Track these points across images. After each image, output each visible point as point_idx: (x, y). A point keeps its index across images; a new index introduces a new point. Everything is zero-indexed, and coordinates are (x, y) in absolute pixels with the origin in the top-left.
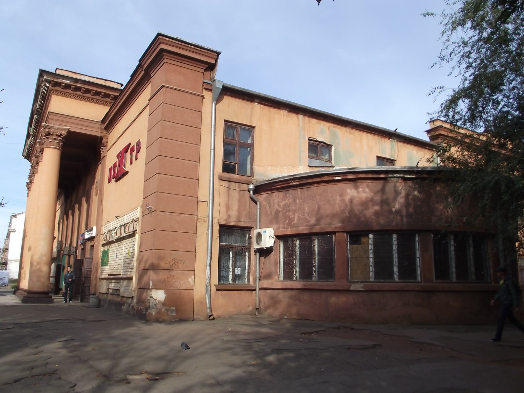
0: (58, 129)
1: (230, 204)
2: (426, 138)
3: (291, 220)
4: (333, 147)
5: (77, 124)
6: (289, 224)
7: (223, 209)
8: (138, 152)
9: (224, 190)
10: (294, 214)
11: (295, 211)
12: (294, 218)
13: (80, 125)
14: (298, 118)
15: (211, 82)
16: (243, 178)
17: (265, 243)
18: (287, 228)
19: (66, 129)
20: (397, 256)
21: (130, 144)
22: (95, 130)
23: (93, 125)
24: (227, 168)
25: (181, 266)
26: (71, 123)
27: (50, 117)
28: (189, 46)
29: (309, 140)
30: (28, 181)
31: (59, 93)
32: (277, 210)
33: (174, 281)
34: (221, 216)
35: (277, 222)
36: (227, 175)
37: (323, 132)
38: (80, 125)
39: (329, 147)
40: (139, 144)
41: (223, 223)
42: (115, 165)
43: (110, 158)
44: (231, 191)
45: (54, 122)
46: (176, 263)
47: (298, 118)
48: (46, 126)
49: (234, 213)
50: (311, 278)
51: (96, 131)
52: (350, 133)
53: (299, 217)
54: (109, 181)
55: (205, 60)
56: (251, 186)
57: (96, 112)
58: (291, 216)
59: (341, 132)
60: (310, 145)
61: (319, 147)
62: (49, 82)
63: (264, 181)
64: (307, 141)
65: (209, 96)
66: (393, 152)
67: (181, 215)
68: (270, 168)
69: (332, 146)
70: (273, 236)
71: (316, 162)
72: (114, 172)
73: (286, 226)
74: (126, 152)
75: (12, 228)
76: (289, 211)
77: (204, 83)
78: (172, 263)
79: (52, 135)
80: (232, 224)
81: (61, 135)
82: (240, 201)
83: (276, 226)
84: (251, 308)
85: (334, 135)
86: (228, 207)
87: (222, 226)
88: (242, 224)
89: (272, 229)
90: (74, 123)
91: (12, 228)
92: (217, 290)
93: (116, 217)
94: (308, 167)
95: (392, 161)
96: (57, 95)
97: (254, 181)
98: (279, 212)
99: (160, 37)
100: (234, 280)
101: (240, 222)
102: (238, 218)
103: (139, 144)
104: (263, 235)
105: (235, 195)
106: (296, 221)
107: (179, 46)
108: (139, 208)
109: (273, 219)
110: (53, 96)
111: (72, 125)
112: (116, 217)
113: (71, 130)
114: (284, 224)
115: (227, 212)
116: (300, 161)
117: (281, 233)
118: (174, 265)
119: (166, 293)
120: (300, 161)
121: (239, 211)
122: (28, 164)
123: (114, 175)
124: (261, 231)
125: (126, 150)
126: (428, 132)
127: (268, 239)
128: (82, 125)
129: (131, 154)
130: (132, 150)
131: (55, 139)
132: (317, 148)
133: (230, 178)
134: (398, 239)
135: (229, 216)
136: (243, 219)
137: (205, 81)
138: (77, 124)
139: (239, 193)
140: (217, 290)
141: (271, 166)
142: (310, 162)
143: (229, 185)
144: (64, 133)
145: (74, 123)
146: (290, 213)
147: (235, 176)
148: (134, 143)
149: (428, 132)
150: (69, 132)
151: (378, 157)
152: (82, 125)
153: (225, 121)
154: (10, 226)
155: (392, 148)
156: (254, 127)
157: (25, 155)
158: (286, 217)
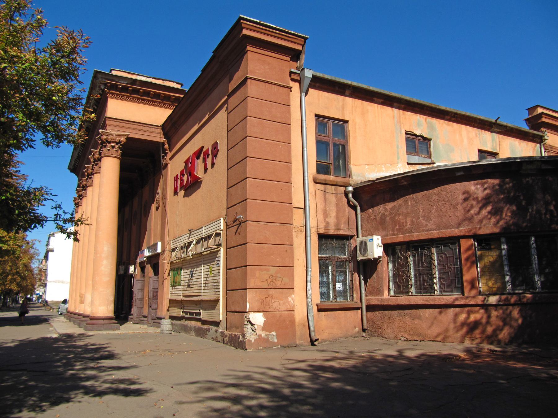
0: (116, 135)
1: (327, 209)
2: (525, 128)
3: (402, 225)
4: (432, 142)
5: (137, 129)
6: (400, 231)
7: (321, 216)
8: (215, 155)
9: (319, 194)
10: (406, 218)
11: (406, 215)
12: (406, 222)
13: (139, 130)
14: (393, 111)
15: (299, 72)
16: (339, 180)
17: (373, 252)
18: (397, 234)
19: (125, 135)
20: (536, 262)
21: (203, 147)
22: (155, 135)
23: (154, 130)
24: (322, 169)
25: (279, 283)
26: (130, 128)
27: (107, 122)
28: (274, 31)
29: (406, 134)
30: (76, 196)
31: (115, 97)
32: (383, 214)
33: (273, 301)
34: (316, 224)
35: (384, 229)
36: (323, 177)
37: (420, 124)
38: (139, 130)
39: (426, 140)
40: (215, 146)
41: (322, 231)
42: (182, 174)
43: (174, 166)
44: (327, 195)
45: (111, 128)
46: (274, 281)
47: (393, 111)
48: (103, 132)
49: (332, 220)
50: (407, 292)
51: (158, 137)
52: (448, 125)
53: (412, 221)
54: (176, 193)
55: (291, 47)
56: (350, 189)
57: (158, 115)
58: (402, 221)
59: (437, 123)
60: (407, 139)
61: (417, 142)
62: (105, 84)
63: (362, 183)
64: (404, 135)
65: (295, 86)
66: (495, 145)
67: (275, 224)
68: (367, 167)
69: (430, 140)
70: (381, 245)
71: (415, 159)
72: (182, 180)
73: (396, 233)
74: (198, 158)
75: (50, 247)
76: (399, 214)
77: (291, 73)
78: (269, 280)
79: (110, 142)
80: (331, 232)
81: (120, 142)
82: (337, 205)
83: (384, 233)
84: (357, 329)
85: (431, 128)
86: (326, 214)
87: (322, 237)
88: (342, 232)
89: (379, 237)
90: (133, 129)
91: (50, 247)
92: (319, 310)
93: (189, 230)
94: (407, 165)
95: (494, 154)
96: (113, 98)
97: (352, 183)
98: (386, 216)
99: (242, 21)
100: (335, 298)
101: (339, 230)
102: (337, 225)
103: (215, 146)
104: (369, 244)
105: (332, 199)
106: (408, 226)
107: (263, 31)
108: (222, 219)
109: (379, 226)
110: (109, 99)
111: (131, 131)
112: (189, 230)
113: (132, 136)
114: (393, 230)
115: (325, 220)
116: (398, 158)
117: (391, 239)
118: (272, 283)
119: (265, 316)
120: (398, 158)
121: (337, 217)
122: (74, 179)
123: (181, 184)
124: (366, 239)
125: (197, 154)
126: (527, 120)
127: (376, 249)
128: (142, 130)
129: (205, 160)
130: (206, 155)
131: (113, 147)
132: (417, 143)
133: (325, 180)
134: (536, 241)
135: (327, 224)
136: (342, 226)
137: (293, 70)
138: (137, 129)
139: (336, 197)
140: (319, 310)
141: (368, 165)
142: (408, 159)
143: (325, 189)
144: (123, 139)
145: (133, 129)
146: (400, 217)
147: (331, 178)
148: (208, 147)
149: (527, 120)
150: (129, 139)
151: (480, 151)
152: (142, 130)
153: (316, 116)
154: (47, 245)
155: (493, 140)
156: (347, 122)
157: (71, 167)
158: (395, 223)
